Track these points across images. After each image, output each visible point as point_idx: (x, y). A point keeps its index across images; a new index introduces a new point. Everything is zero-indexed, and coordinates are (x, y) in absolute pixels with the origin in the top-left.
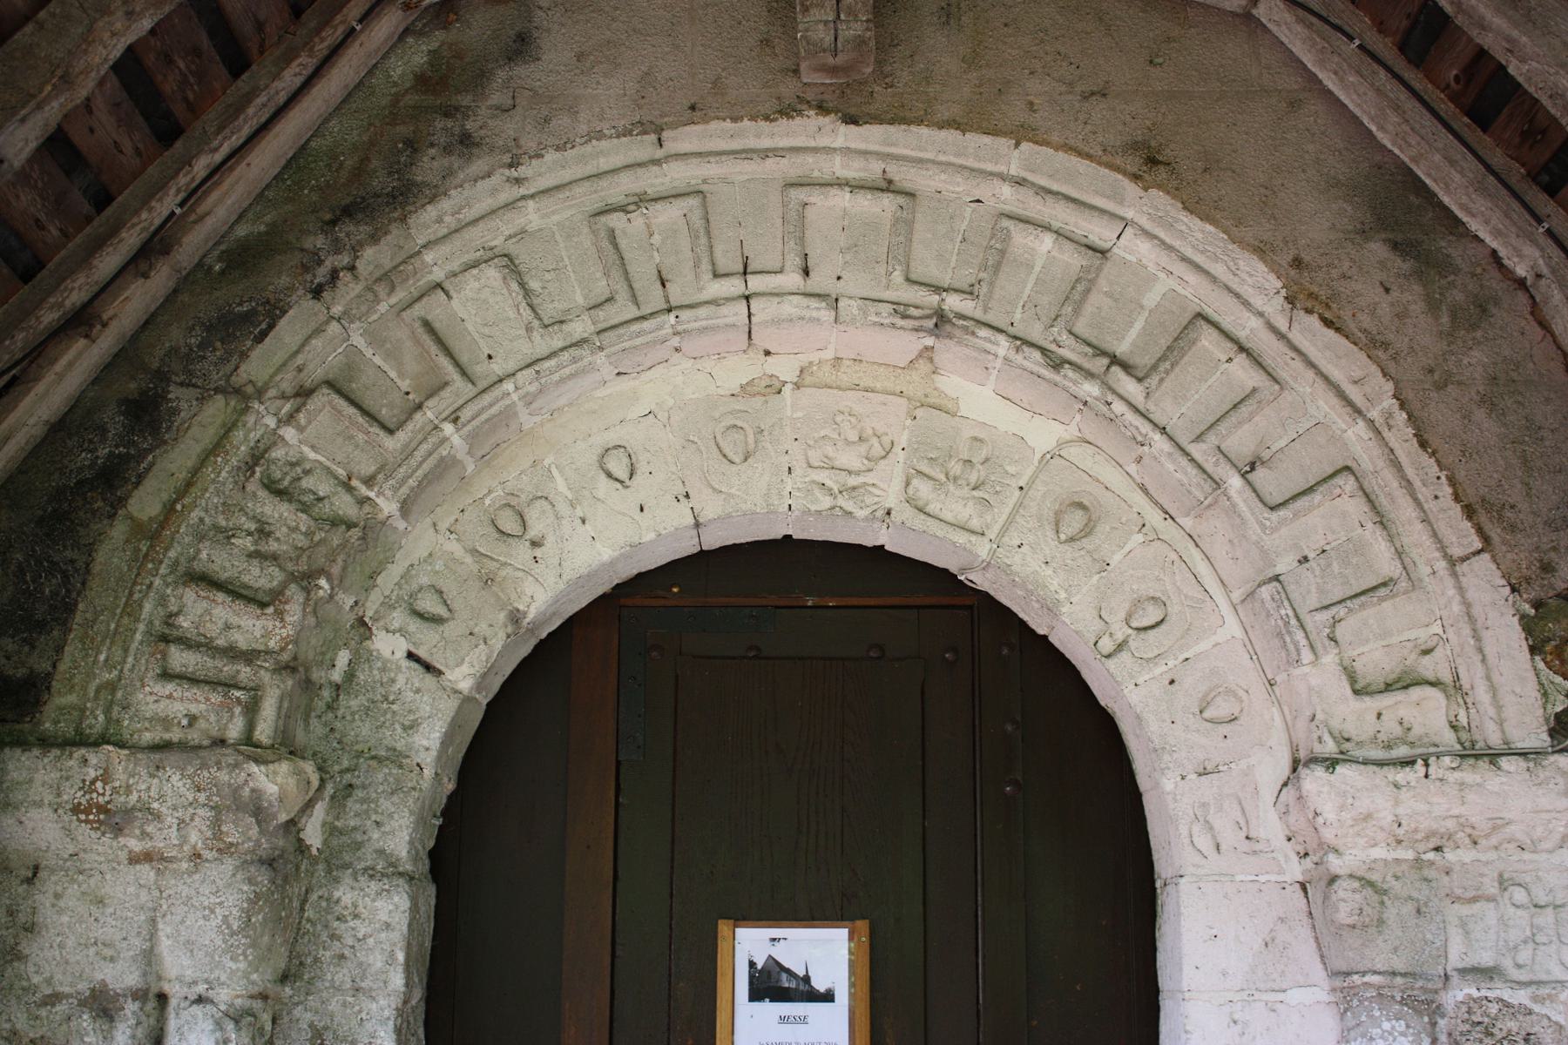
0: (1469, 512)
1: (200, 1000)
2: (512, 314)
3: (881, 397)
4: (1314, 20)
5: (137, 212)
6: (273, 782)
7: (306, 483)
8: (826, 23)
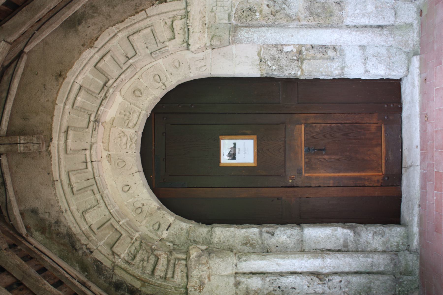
0: (137, 13)
1: (236, 266)
2: (95, 211)
3: (111, 133)
4: (30, 40)
5: (78, 287)
6: (194, 254)
7: (132, 252)
8: (33, 145)
